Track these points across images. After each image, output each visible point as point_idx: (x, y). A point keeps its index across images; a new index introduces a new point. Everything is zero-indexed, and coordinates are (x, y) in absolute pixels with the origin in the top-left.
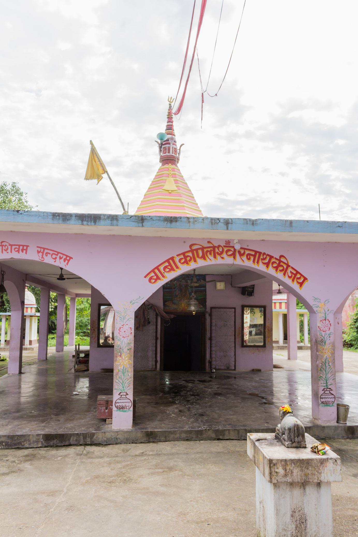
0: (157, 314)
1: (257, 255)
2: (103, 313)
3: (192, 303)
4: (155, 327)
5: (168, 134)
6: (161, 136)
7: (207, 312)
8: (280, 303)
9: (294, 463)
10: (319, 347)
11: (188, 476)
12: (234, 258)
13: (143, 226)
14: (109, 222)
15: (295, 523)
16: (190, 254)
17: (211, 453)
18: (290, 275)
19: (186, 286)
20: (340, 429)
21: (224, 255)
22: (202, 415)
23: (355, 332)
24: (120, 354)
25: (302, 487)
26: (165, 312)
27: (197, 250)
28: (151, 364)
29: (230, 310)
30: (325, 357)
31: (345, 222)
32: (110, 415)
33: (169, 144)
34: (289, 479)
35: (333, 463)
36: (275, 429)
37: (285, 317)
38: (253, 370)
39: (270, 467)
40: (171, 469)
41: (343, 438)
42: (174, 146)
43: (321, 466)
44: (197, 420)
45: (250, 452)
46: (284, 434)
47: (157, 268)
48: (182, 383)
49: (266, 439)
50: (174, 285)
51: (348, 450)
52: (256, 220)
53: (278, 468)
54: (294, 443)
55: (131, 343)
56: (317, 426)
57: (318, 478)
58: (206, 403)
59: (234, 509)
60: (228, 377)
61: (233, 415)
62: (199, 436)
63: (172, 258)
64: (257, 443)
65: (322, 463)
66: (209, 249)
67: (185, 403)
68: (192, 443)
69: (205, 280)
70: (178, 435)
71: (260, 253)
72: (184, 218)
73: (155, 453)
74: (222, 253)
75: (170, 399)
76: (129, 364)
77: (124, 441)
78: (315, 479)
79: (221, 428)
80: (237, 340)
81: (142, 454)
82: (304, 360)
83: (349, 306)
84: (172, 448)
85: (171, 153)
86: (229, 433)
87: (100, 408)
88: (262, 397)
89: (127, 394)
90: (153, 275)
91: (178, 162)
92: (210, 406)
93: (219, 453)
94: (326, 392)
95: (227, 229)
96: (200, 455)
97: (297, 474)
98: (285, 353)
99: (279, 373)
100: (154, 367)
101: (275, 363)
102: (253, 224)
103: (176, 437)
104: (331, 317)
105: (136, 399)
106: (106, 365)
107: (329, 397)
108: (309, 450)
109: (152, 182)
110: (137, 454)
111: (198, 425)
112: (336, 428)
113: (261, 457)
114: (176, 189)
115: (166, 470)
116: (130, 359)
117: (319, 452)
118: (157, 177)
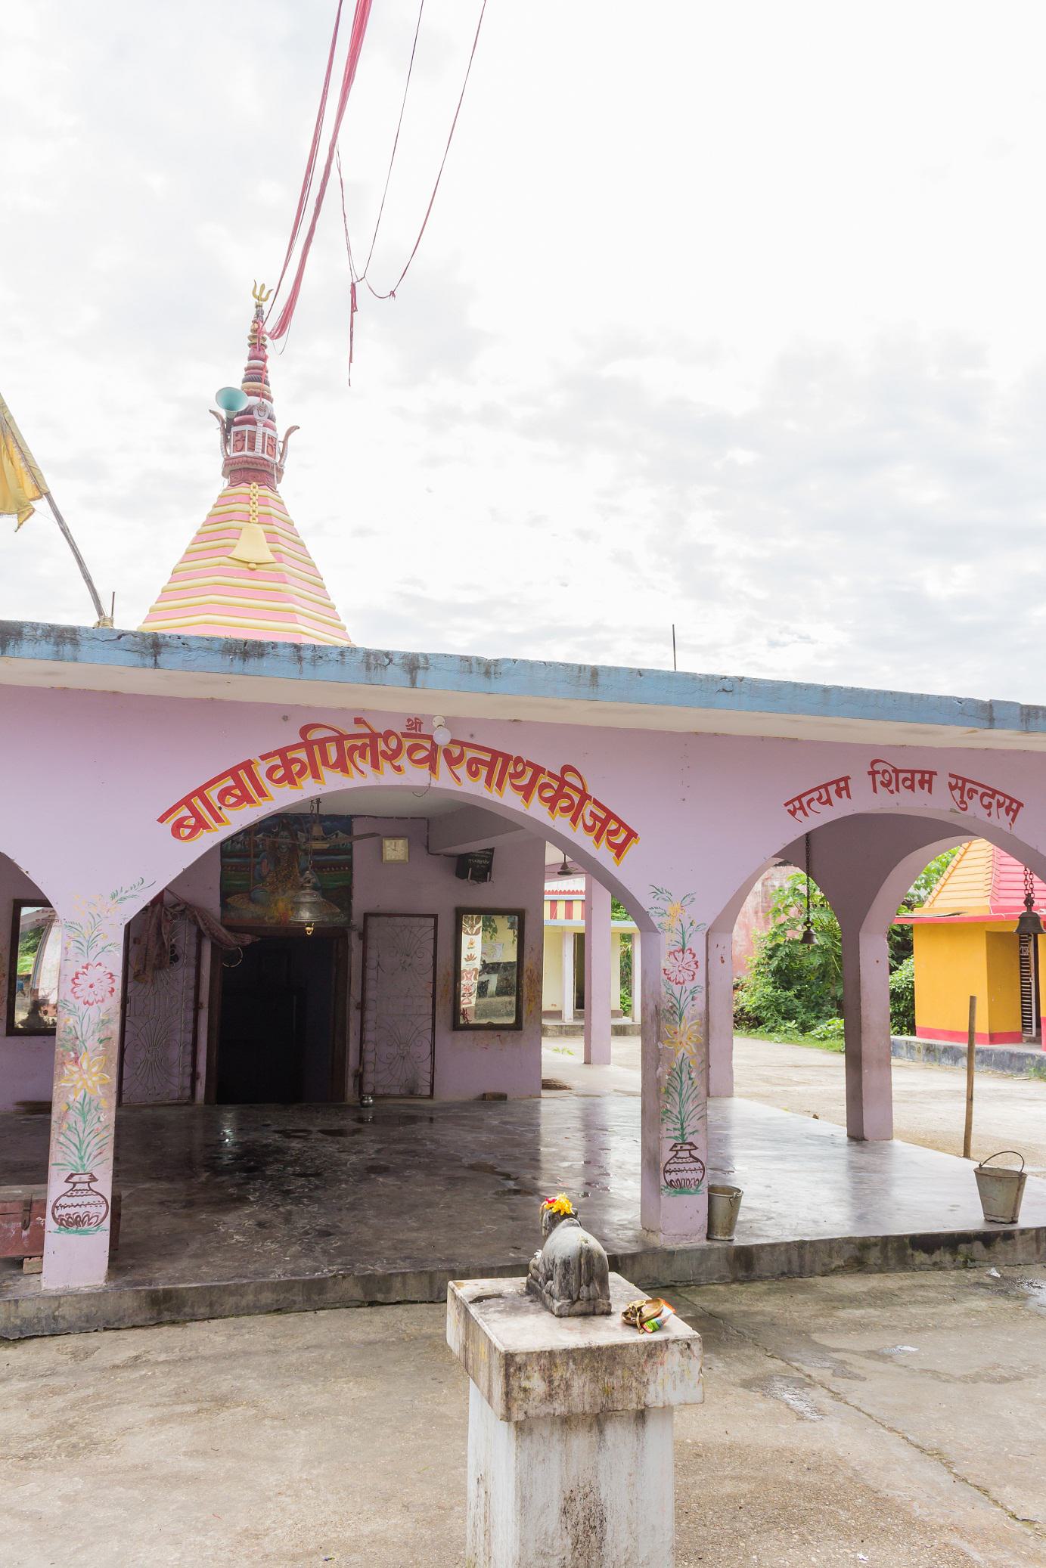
0: (199, 931)
1: (498, 765)
2: (28, 928)
3: (303, 900)
4: (192, 971)
5: (249, 394)
6: (228, 398)
7: (352, 927)
8: (569, 902)
9: (574, 1360)
10: (666, 1027)
11: (274, 1418)
12: (433, 769)
13: (156, 665)
14: (47, 648)
15: (573, 1531)
16: (302, 755)
17: (348, 1344)
18: (590, 822)
19: (294, 849)
20: (714, 1257)
21: (403, 760)
22: (325, 1234)
23: (768, 983)
24: (73, 1055)
25: (595, 1429)
26: (229, 928)
27: (322, 743)
28: (178, 1082)
29: (422, 921)
30: (679, 1055)
31: (742, 679)
32: (37, 1246)
33: (254, 423)
34: (559, 1408)
35: (682, 1353)
36: (528, 1266)
37: (581, 941)
38: (484, 1097)
39: (507, 1376)
40: (221, 1401)
41: (722, 1280)
42: (269, 431)
43: (649, 1364)
44: (309, 1250)
45: (453, 1334)
46: (549, 1278)
47: (200, 793)
48: (273, 1139)
49: (499, 1296)
50: (256, 845)
51: (732, 1313)
52: (497, 662)
53: (528, 1378)
54: (578, 1304)
55: (109, 1021)
56: (653, 1252)
57: (639, 1398)
58: (340, 1197)
59: (406, 1507)
60: (412, 1119)
61: (418, 1230)
62: (316, 1298)
63: (247, 766)
64: (474, 1310)
65: (650, 1356)
66: (359, 742)
67: (278, 1199)
68: (291, 1319)
69: (349, 831)
70: (251, 1297)
71: (507, 758)
72: (285, 645)
73: (176, 1355)
74: (396, 753)
75: (231, 1190)
76: (102, 1086)
77: (80, 1324)
78: (631, 1401)
79: (379, 1269)
80: (439, 1009)
81: (135, 1362)
82: (624, 1065)
83: (756, 912)
84: (230, 1337)
85: (258, 452)
86: (404, 1284)
87: (6, 1226)
88: (507, 1175)
89: (93, 1179)
90: (186, 816)
91: (279, 481)
92: (353, 1207)
93: (370, 1343)
94: (681, 1154)
95: (413, 684)
96: (315, 1354)
97: (582, 1390)
98: (575, 1047)
99: (557, 1102)
100: (188, 1092)
101: (546, 1074)
102: (487, 673)
103: (244, 1303)
104: (697, 944)
105: (124, 1193)
106: (30, 1092)
107: (687, 1166)
108: (617, 1319)
109: (199, 533)
110: (117, 1362)
111: (311, 1263)
112: (704, 1253)
113: (483, 1349)
114: (271, 558)
115: (206, 1405)
116: (105, 1069)
117: (645, 1325)
118: (213, 519)
